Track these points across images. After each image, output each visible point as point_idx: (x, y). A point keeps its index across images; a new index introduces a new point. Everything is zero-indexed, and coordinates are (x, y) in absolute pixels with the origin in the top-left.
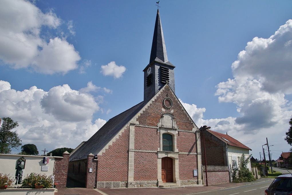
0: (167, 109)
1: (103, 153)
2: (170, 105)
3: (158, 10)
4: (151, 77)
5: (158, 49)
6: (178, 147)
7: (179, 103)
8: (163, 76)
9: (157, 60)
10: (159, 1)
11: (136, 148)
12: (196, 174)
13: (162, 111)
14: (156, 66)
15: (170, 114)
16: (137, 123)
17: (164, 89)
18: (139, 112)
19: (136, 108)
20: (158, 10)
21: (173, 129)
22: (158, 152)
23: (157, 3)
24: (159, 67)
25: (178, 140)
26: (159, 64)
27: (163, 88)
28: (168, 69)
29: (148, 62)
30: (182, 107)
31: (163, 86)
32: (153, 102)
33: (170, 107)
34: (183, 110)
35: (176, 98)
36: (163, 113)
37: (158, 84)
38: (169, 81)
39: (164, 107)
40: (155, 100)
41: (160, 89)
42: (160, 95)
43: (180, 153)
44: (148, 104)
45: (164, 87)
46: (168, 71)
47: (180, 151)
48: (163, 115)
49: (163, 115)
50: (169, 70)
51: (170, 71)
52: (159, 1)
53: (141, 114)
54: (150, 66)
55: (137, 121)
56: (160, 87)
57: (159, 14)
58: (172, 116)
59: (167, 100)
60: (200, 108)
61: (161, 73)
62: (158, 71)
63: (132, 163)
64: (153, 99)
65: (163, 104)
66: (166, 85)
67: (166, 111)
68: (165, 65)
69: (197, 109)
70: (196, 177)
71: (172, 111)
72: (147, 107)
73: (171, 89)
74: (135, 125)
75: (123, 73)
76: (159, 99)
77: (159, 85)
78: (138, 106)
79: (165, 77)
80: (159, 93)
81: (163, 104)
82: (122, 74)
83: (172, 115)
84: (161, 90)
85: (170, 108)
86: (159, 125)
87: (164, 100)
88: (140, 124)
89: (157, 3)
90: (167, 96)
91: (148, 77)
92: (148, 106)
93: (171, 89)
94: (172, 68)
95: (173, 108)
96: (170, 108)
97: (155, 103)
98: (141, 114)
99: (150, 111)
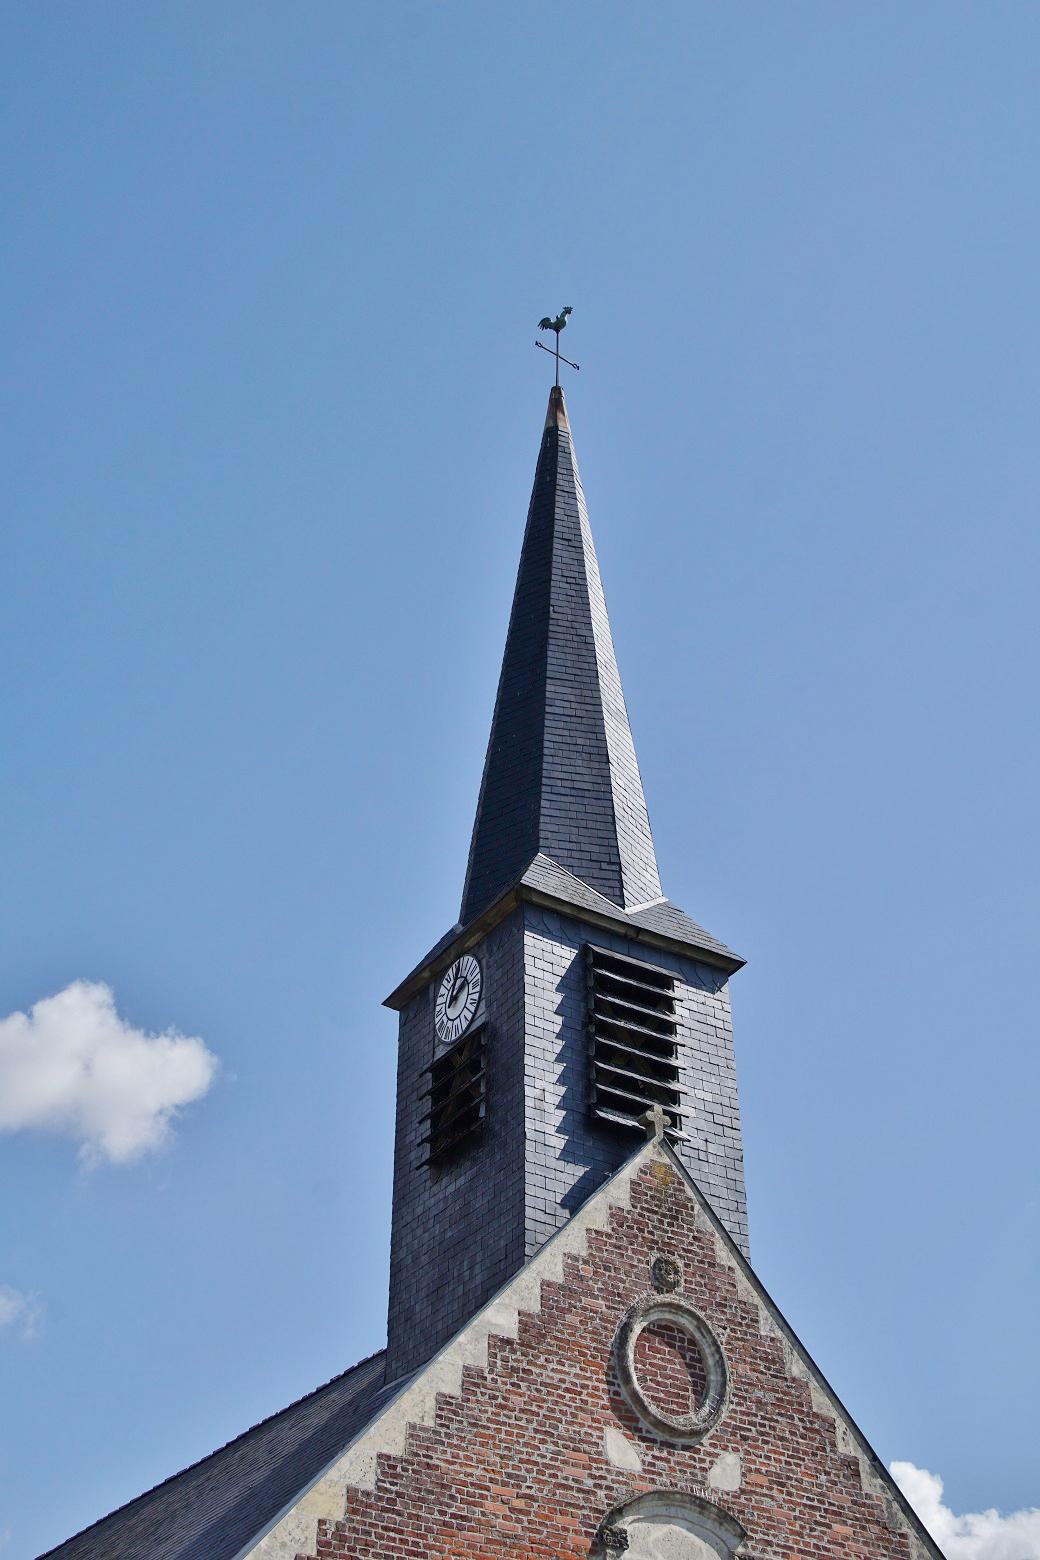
0: (660, 1436)
2: (701, 1393)
3: (556, 391)
4: (475, 1067)
5: (557, 765)
7: (796, 1368)
8: (607, 1054)
9: (544, 876)
10: (568, 311)
13: (600, 1459)
14: (525, 880)
15: (702, 1505)
17: (626, 1205)
19: (291, 1437)
20: (556, 391)
23: (545, 324)
24: (565, 955)
26: (564, 920)
27: (618, 1191)
28: (667, 983)
29: (447, 915)
30: (841, 1426)
31: (615, 1166)
32: (499, 1343)
33: (694, 1418)
34: (851, 1466)
35: (764, 1313)
36: (621, 1492)
37: (559, 1142)
38: (675, 1109)
39: (630, 1416)
41: (574, 1201)
42: (587, 1271)
44: (444, 1373)
45: (629, 1171)
46: (668, 1004)
48: (625, 1524)
49: (625, 1524)
50: (680, 991)
51: (688, 1001)
52: (568, 311)
53: (352, 1495)
54: (471, 942)
56: (576, 1172)
57: (566, 425)
58: (726, 1533)
59: (663, 1332)
60: (979, 1508)
61: (589, 1020)
62: (558, 998)
64: (501, 1315)
65: (618, 1372)
66: (648, 1154)
67: (649, 1468)
68: (635, 937)
69: (957, 1524)
71: (725, 1474)
72: (430, 1404)
73: (707, 1206)
75: (177, 1107)
76: (569, 1318)
77: (567, 1155)
78: (318, 1417)
79: (630, 1062)
80: (574, 1239)
81: (618, 1372)
82: (172, 1119)
83: (724, 1516)
84: (596, 1212)
85: (697, 1434)
87: (626, 1328)
89: (545, 324)
90: (662, 1284)
91: (441, 1069)
92: (444, 1401)
93: (707, 1206)
94: (714, 968)
95: (737, 1436)
96: (697, 1434)
97: (517, 1359)
99: (453, 1464)
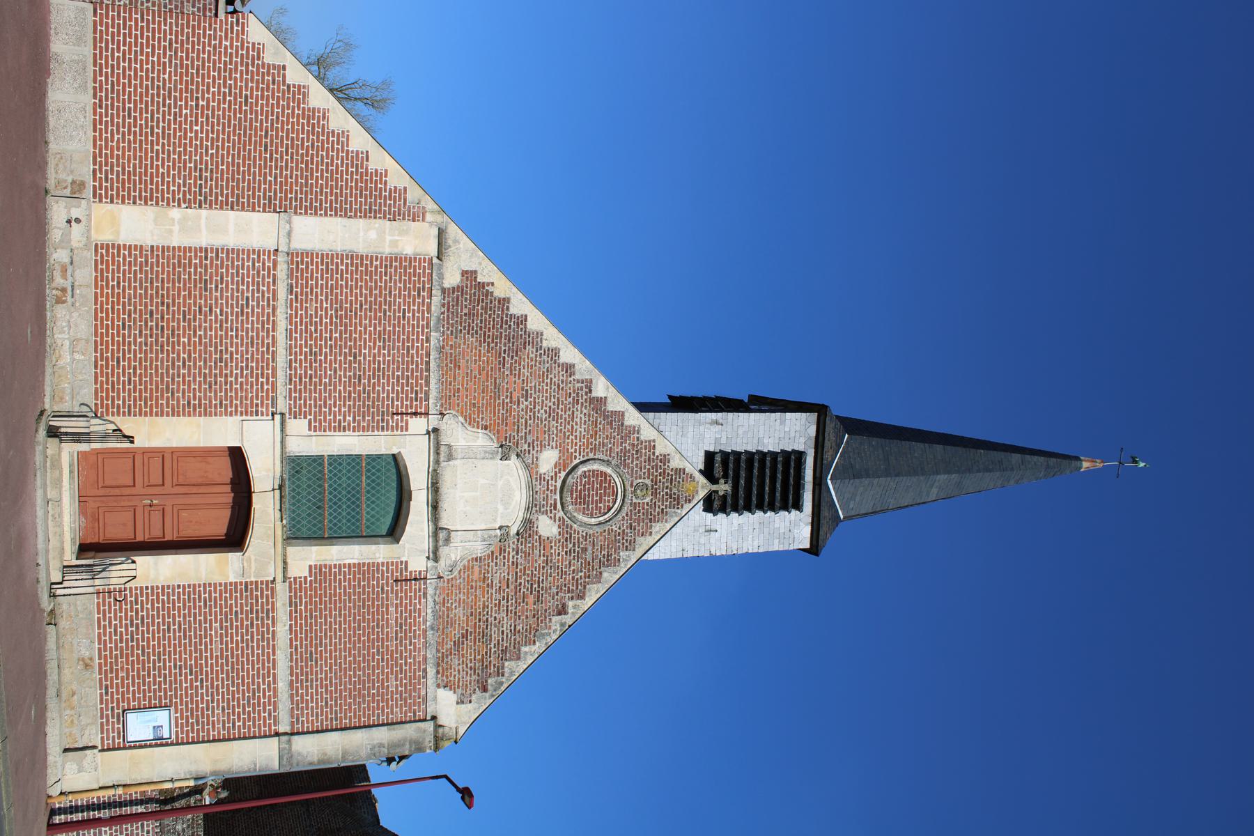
1: (259, 50)
6: (319, 571)
11: (301, 261)
12: (140, 726)
16: (452, 278)
18: (515, 290)
21: (439, 534)
22: (278, 417)
25: (362, 571)
32: (589, 385)
40: (602, 401)
43: (282, 590)
47: (296, 587)
53: (507, 300)
55: (464, 273)
63: (204, 232)
70: (123, 733)
74: (435, 261)
78: (815, 519)
86: (458, 434)
88: (443, 290)
98: (507, 300)
